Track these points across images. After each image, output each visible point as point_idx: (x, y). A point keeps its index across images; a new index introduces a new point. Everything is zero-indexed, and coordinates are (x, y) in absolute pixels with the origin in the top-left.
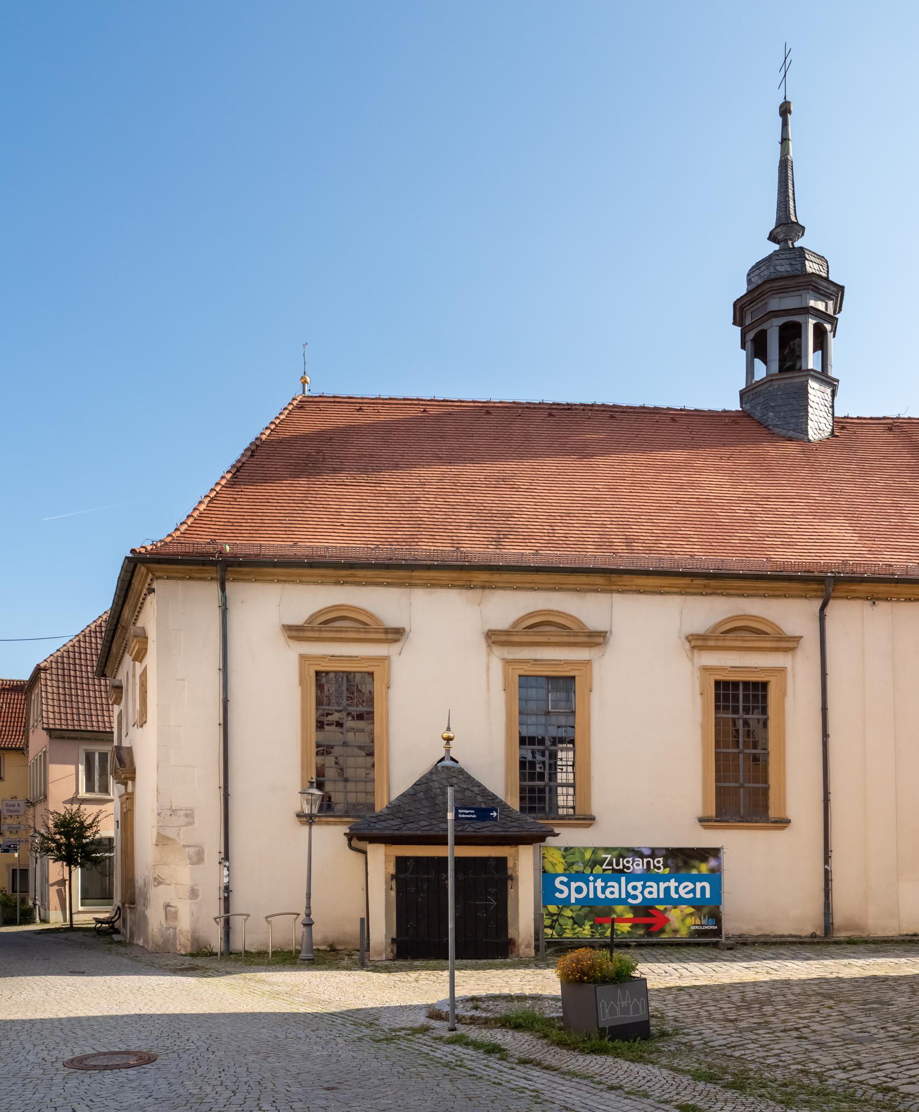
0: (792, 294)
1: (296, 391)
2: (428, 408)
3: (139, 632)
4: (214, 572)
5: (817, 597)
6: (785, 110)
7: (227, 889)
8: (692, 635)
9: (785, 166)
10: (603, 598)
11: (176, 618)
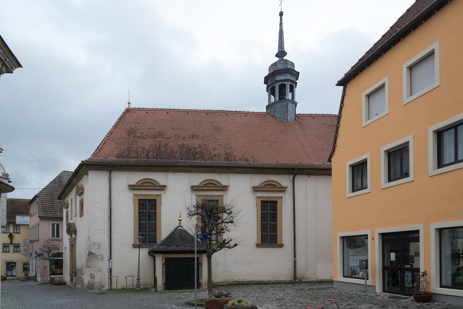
1: (127, 106)
3: (81, 187)
5: (292, 174)
6: (281, 14)
7: (111, 270)
9: (281, 32)
10: (227, 175)
11: (95, 183)
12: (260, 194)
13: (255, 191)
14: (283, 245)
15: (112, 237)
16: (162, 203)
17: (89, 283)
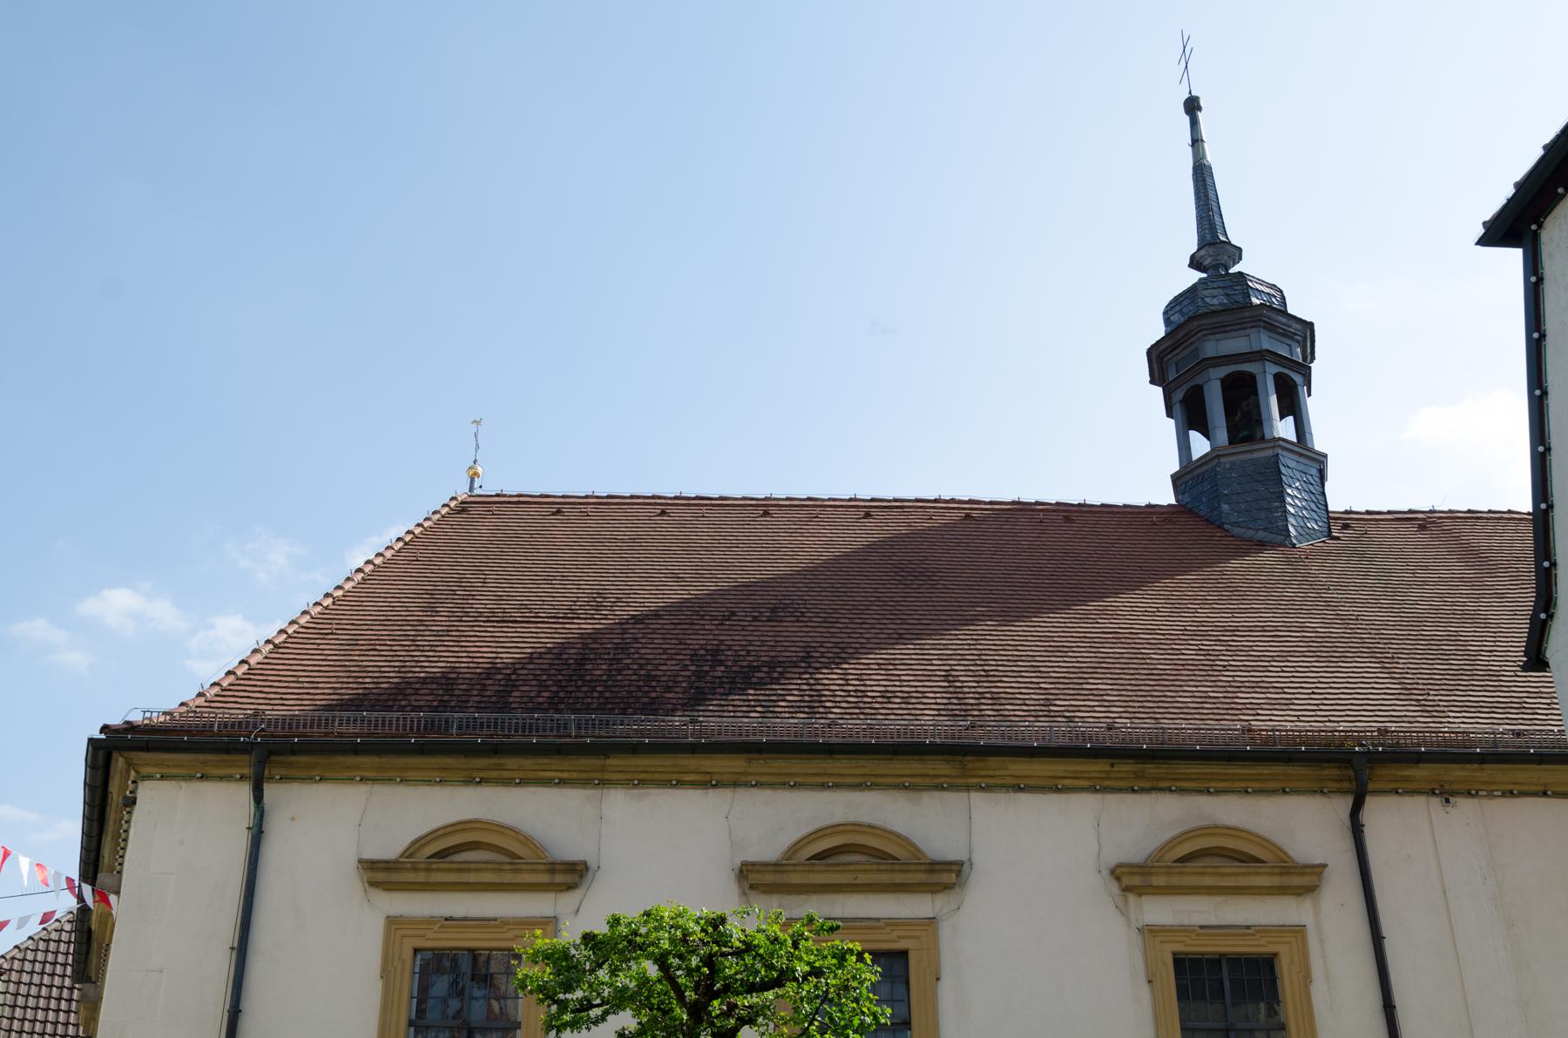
1: (462, 492)
2: (669, 509)
4: (244, 764)
5: (1342, 792)
8: (1119, 866)
9: (1202, 176)
12: (1160, 911)
13: (1127, 889)
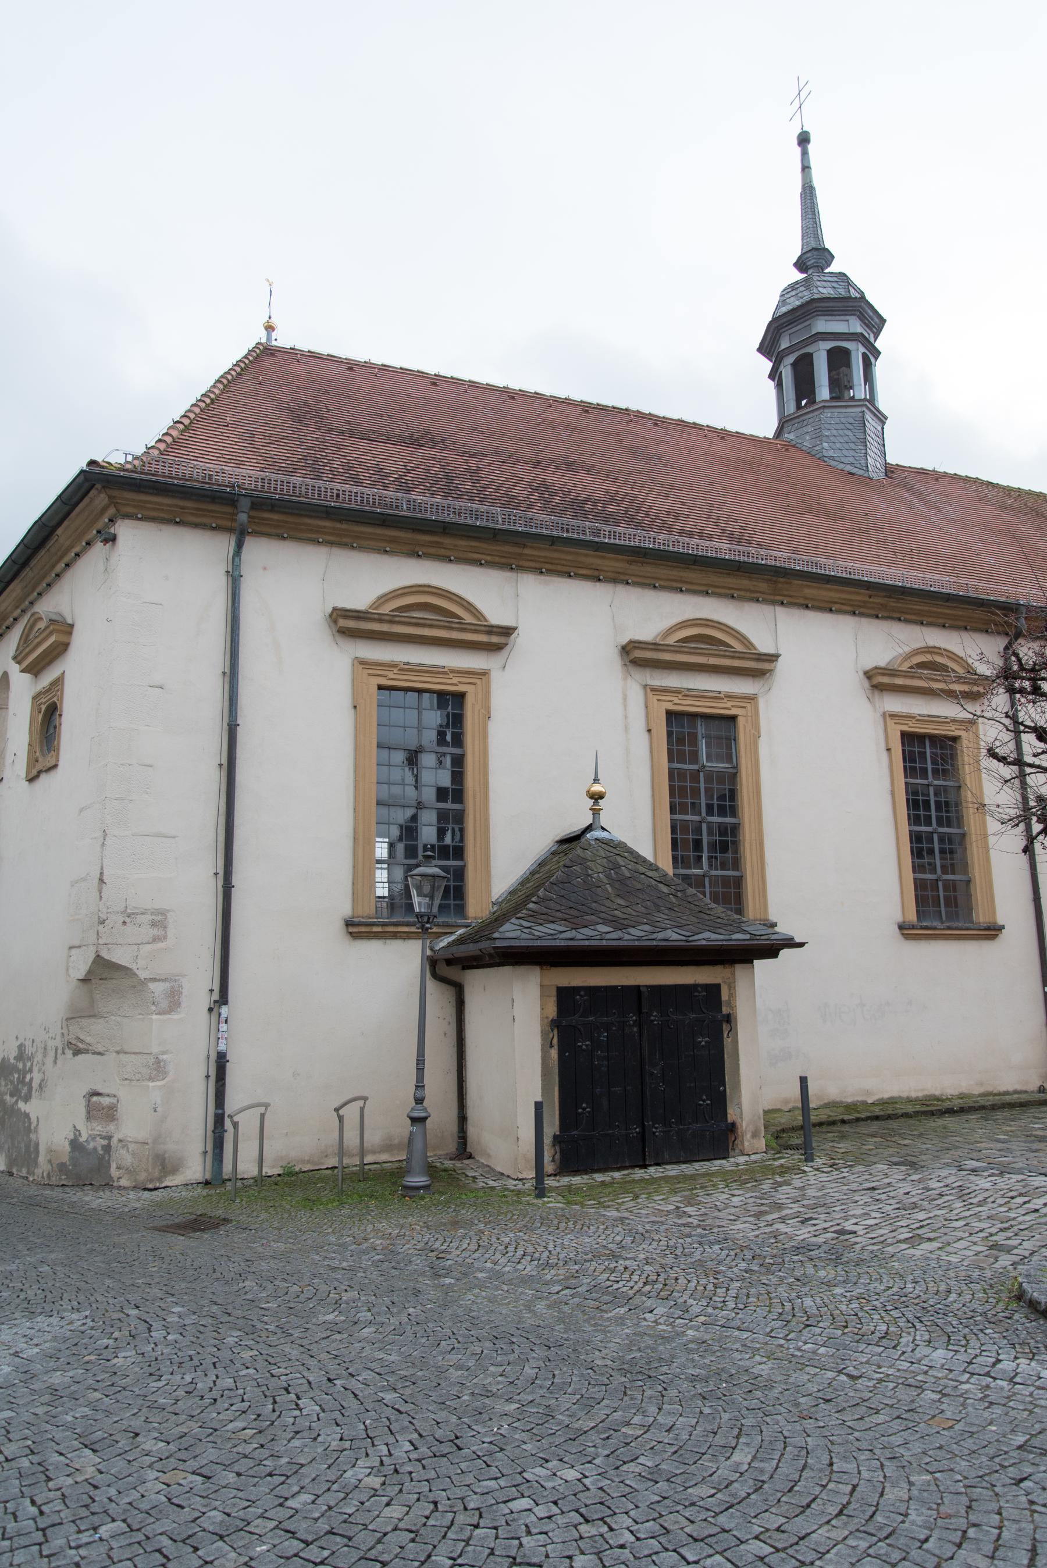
0: (838, 318)
6: (804, 140)
7: (221, 1062)
9: (808, 193)
10: (767, 610)
11: (143, 598)
14: (1001, 928)
15: (235, 880)
16: (494, 713)
17: (75, 1144)
